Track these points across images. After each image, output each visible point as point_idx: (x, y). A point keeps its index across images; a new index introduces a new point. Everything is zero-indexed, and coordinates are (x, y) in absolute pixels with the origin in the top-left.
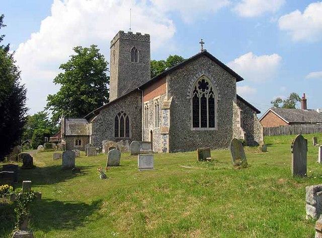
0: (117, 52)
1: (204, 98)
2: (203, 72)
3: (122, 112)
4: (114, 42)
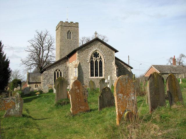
0: (59, 33)
1: (96, 62)
2: (96, 48)
3: (58, 69)
4: (58, 27)
